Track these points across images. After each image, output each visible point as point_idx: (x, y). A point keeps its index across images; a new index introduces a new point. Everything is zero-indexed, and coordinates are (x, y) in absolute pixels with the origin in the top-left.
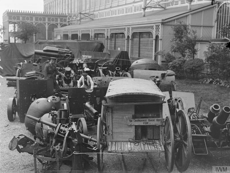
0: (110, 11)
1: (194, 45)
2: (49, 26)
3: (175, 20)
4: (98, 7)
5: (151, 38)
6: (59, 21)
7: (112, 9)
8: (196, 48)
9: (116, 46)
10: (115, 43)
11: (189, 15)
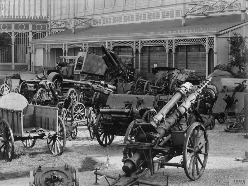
0: (123, 16)
2: (17, 36)
3: (229, 32)
4: (122, 6)
5: (202, 51)
6: (30, 29)
7: (125, 13)
9: (151, 62)
10: (149, 58)
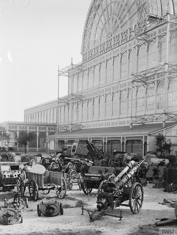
1: (170, 147)
6: (47, 130)
8: (171, 149)
11: (163, 130)
